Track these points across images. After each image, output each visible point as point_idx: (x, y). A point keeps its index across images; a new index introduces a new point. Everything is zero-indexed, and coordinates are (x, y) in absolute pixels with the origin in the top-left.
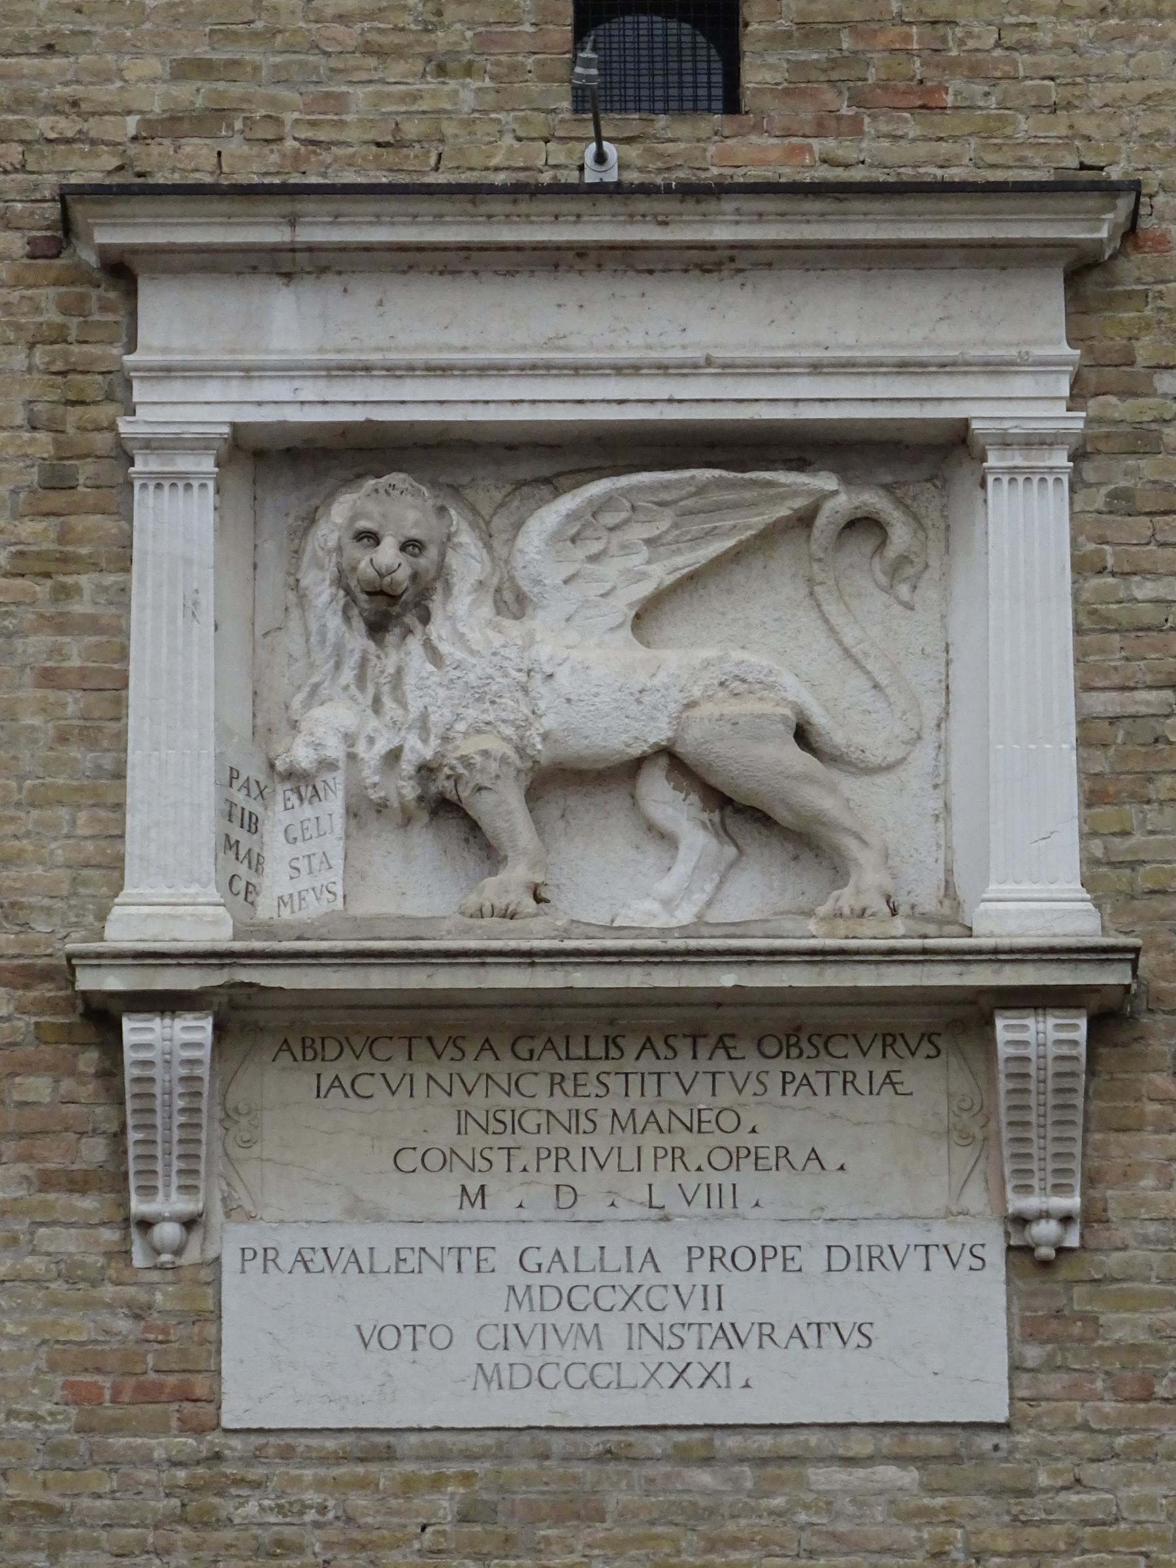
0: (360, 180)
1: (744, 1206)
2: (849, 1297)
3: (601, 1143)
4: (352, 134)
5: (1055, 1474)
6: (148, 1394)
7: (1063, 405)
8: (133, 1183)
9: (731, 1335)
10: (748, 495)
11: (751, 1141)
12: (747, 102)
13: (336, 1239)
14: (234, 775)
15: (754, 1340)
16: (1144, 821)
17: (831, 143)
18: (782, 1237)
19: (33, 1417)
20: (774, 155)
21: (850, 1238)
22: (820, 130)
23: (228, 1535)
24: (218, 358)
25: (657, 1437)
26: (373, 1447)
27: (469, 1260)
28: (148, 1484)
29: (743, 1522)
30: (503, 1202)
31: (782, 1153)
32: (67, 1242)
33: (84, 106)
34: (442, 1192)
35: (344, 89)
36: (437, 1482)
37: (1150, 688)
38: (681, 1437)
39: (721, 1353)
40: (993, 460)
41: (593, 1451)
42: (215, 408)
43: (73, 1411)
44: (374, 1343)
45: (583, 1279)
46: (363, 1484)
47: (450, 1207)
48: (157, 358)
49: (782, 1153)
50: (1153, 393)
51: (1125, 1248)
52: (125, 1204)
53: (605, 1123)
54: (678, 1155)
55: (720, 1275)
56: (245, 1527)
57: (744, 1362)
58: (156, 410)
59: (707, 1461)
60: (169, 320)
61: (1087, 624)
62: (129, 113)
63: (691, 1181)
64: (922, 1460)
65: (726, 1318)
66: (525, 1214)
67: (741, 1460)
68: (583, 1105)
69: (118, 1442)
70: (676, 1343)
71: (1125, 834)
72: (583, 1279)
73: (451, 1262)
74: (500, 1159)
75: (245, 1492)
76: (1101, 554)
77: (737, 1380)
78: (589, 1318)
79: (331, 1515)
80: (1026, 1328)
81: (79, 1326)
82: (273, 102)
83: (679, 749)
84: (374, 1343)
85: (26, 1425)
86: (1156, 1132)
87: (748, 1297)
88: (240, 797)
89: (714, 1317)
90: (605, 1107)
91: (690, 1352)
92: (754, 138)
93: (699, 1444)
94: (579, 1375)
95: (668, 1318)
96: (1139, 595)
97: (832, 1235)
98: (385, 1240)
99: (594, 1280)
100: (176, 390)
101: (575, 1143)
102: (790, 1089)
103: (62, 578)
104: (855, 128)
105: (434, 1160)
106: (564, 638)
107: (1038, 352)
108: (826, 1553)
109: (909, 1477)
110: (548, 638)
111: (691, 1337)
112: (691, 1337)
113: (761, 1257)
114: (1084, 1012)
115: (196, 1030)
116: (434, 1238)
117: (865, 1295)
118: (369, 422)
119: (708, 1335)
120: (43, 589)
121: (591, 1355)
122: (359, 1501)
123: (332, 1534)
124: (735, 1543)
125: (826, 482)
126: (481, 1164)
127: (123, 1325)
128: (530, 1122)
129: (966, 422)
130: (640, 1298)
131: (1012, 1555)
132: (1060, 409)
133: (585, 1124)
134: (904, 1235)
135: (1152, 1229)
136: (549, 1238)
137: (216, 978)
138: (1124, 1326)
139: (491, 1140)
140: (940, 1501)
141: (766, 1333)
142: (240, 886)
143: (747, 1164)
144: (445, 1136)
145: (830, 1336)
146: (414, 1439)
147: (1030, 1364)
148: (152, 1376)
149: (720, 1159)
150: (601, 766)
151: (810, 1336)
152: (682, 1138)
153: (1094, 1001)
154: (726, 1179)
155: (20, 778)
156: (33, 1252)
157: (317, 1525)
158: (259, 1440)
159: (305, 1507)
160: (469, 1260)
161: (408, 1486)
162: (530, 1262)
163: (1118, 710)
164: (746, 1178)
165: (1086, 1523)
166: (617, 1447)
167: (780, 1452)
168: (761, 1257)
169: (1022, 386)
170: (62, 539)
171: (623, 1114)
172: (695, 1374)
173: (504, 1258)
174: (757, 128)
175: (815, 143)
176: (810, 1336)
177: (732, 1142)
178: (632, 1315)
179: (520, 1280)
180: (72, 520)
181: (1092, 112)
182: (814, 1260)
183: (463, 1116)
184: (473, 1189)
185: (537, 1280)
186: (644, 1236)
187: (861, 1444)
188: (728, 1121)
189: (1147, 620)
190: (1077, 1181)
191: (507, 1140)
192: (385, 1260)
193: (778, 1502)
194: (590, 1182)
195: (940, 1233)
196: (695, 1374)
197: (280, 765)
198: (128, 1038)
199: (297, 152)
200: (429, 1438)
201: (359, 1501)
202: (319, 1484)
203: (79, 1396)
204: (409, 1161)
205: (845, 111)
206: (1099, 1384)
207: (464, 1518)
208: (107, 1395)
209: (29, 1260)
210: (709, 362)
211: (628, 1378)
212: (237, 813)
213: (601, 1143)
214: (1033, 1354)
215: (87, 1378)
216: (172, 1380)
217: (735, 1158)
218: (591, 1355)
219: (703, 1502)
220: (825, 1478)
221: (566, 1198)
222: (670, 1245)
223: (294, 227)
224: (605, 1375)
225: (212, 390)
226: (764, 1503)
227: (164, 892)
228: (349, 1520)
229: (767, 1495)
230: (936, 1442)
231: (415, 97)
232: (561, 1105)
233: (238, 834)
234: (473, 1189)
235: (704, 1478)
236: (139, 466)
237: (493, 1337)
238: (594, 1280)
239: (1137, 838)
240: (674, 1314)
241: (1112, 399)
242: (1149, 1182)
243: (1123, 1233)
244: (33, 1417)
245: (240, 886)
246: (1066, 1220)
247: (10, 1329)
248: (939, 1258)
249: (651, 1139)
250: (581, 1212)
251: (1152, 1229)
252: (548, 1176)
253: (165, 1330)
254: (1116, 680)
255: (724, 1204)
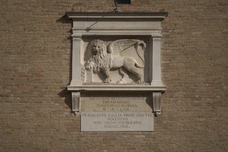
0: (98, 12)
1: (129, 110)
2: (138, 119)
3: (116, 104)
4: (93, 6)
5: (158, 136)
6: (74, 128)
7: (160, 33)
8: (73, 108)
9: (128, 123)
10: (130, 42)
11: (130, 104)
12: (131, 3)
13: (91, 113)
14: (82, 69)
15: (130, 123)
16: (167, 74)
17: (139, 7)
18: (133, 113)
19: (63, 130)
20: (133, 8)
21: (139, 113)
22: (138, 6)
23: (81, 141)
24: (80, 28)
25: (121, 132)
26: (95, 133)
27: (104, 115)
28: (74, 137)
29: (129, 140)
30: (107, 109)
31: (133, 105)
32: (66, 113)
33: (68, 3)
34: (101, 109)
35: (92, 1)
36: (101, 137)
37: (168, 61)
38: (123, 132)
39: (127, 124)
40: (154, 39)
41: (115, 134)
42: (80, 33)
43: (67, 130)
44: (95, 123)
45: (114, 117)
46: (94, 137)
47: (102, 110)
48: (75, 28)
49: (133, 105)
50: (169, 32)
51: (165, 115)
52: (72, 110)
53: (117, 102)
54: (123, 105)
55: (127, 117)
56: (83, 141)
57: (129, 125)
58: (75, 33)
59: (125, 134)
60: (76, 24)
61: (162, 55)
62: (72, 3)
63: (124, 108)
64: (145, 135)
65: (128, 121)
66: (109, 111)
67: (129, 134)
68: (114, 101)
69: (71, 133)
70: (123, 123)
71: (165, 75)
72: (114, 117)
73: (102, 116)
74: (107, 106)
75: (83, 137)
76: (163, 48)
77: (129, 127)
78: (115, 121)
79: (91, 140)
80: (156, 122)
81: (68, 122)
82: (86, 2)
83: (124, 67)
84: (95, 123)
85: (63, 131)
86: (168, 103)
87: (130, 119)
88: (83, 71)
89: (127, 121)
90: (117, 101)
91: (124, 124)
92: (131, 7)
93: (125, 133)
94: (114, 127)
95: (122, 121)
96: (167, 52)
97: (138, 113)
98: (96, 113)
99: (115, 117)
100: (77, 31)
101: (114, 104)
102: (134, 99)
103: (66, 49)
104: (141, 5)
105: (101, 106)
106: (116, 56)
107: (158, 28)
108: (137, 143)
109: (144, 136)
110: (112, 56)
111: (124, 123)
112: (124, 123)
113: (131, 115)
114: (80, 92)
115: (78, 94)
116: (100, 113)
117: (140, 120)
118: (95, 35)
119: (126, 123)
120: (64, 50)
121: (115, 125)
122: (94, 138)
123: (91, 141)
124: (128, 142)
125: (138, 40)
126: (105, 106)
127: (72, 121)
128: (110, 102)
129: (151, 35)
130: (120, 119)
131: (154, 144)
132: (160, 34)
133: (115, 102)
134: (144, 113)
135: (167, 113)
136: (111, 113)
137: (81, 89)
138: (165, 122)
139: (106, 104)
140: (147, 139)
141: (131, 122)
142: (83, 80)
143: (130, 106)
144: (102, 103)
145: (137, 123)
146: (99, 132)
147: (156, 126)
148: (74, 126)
149: (127, 106)
150: (127, 69)
151: (135, 123)
152: (124, 104)
153: (162, 91)
154: (128, 108)
155: (62, 69)
156: (64, 114)
157: (89, 140)
158: (85, 132)
159: (89, 139)
160: (104, 115)
161: (98, 137)
162: (109, 116)
163: (165, 63)
164: (130, 108)
165: (161, 141)
166: (118, 133)
167: (132, 134)
168: (131, 115)
169: (156, 31)
170: (66, 45)
171: (118, 102)
172: (125, 126)
173: (107, 115)
174: (132, 6)
175: (137, 7)
176: (135, 123)
177: (128, 104)
178: (119, 121)
179: (109, 117)
180: (67, 44)
181: (163, 4)
182: (136, 115)
183: (103, 102)
184: (104, 108)
185: (110, 117)
186: (120, 113)
187: (140, 133)
188: (128, 102)
189: (168, 54)
190: (160, 108)
191: (108, 104)
192: (96, 115)
193: (132, 138)
194: (115, 108)
195: (148, 113)
196: (125, 126)
197: (87, 68)
198: (72, 95)
199: (88, 8)
200: (100, 132)
201: (94, 138)
202: (90, 137)
203: (67, 128)
204: (98, 106)
205: (140, 4)
206: (162, 128)
207: (103, 140)
208: (70, 128)
209: (63, 115)
210: (127, 29)
211: (118, 127)
212: (83, 73)
213: (116, 104)
214: (156, 125)
215: (68, 126)
216: (76, 127)
217: (129, 106)
218: (115, 125)
219: (125, 138)
220: (137, 136)
221: (113, 109)
222: (123, 114)
223: (86, 16)
224: (116, 126)
225: (80, 31)
226: (131, 139)
227: (76, 80)
228: (93, 140)
229: (131, 138)
230: (147, 133)
231: (100, 2)
232: (112, 101)
233: (82, 74)
234: (104, 108)
235: (125, 136)
236: (73, 39)
237: (106, 123)
238: (115, 117)
239: (166, 75)
240: (123, 121)
241: (165, 33)
242: (167, 108)
243: (165, 113)
244: (63, 130)
245: (83, 80)
246: (159, 112)
247: (61, 122)
248: (147, 115)
249: (121, 104)
250: (114, 111)
251: (167, 113)
252: (111, 107)
253: (76, 122)
254: (165, 60)
255: (127, 110)
